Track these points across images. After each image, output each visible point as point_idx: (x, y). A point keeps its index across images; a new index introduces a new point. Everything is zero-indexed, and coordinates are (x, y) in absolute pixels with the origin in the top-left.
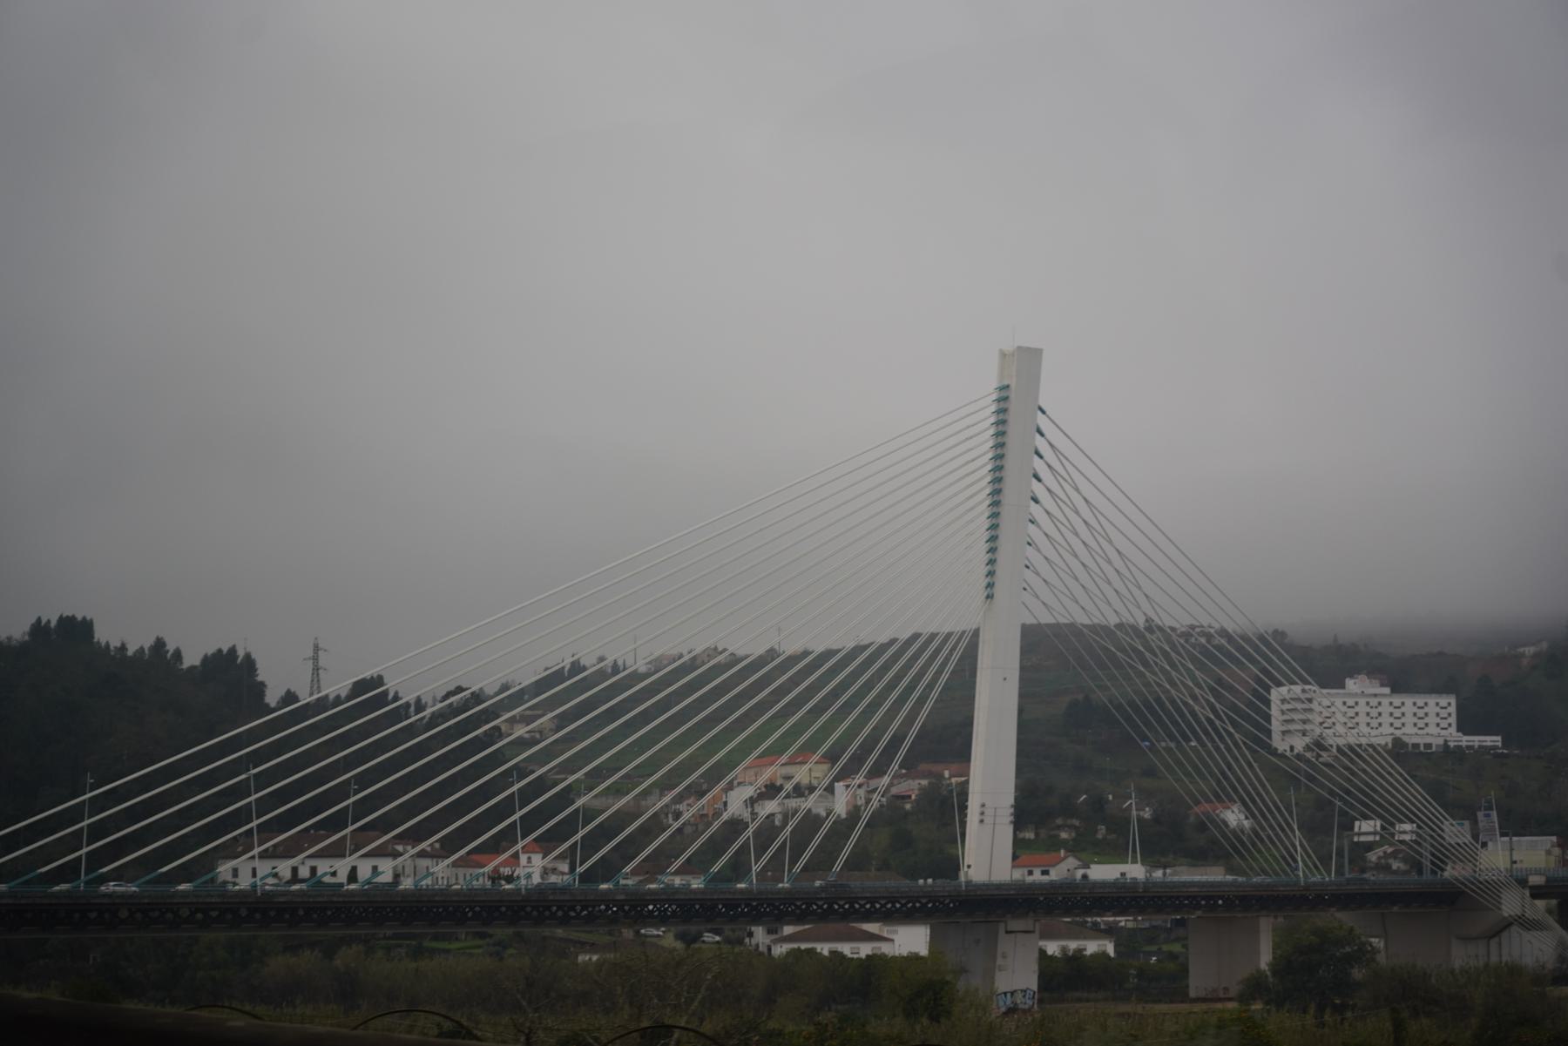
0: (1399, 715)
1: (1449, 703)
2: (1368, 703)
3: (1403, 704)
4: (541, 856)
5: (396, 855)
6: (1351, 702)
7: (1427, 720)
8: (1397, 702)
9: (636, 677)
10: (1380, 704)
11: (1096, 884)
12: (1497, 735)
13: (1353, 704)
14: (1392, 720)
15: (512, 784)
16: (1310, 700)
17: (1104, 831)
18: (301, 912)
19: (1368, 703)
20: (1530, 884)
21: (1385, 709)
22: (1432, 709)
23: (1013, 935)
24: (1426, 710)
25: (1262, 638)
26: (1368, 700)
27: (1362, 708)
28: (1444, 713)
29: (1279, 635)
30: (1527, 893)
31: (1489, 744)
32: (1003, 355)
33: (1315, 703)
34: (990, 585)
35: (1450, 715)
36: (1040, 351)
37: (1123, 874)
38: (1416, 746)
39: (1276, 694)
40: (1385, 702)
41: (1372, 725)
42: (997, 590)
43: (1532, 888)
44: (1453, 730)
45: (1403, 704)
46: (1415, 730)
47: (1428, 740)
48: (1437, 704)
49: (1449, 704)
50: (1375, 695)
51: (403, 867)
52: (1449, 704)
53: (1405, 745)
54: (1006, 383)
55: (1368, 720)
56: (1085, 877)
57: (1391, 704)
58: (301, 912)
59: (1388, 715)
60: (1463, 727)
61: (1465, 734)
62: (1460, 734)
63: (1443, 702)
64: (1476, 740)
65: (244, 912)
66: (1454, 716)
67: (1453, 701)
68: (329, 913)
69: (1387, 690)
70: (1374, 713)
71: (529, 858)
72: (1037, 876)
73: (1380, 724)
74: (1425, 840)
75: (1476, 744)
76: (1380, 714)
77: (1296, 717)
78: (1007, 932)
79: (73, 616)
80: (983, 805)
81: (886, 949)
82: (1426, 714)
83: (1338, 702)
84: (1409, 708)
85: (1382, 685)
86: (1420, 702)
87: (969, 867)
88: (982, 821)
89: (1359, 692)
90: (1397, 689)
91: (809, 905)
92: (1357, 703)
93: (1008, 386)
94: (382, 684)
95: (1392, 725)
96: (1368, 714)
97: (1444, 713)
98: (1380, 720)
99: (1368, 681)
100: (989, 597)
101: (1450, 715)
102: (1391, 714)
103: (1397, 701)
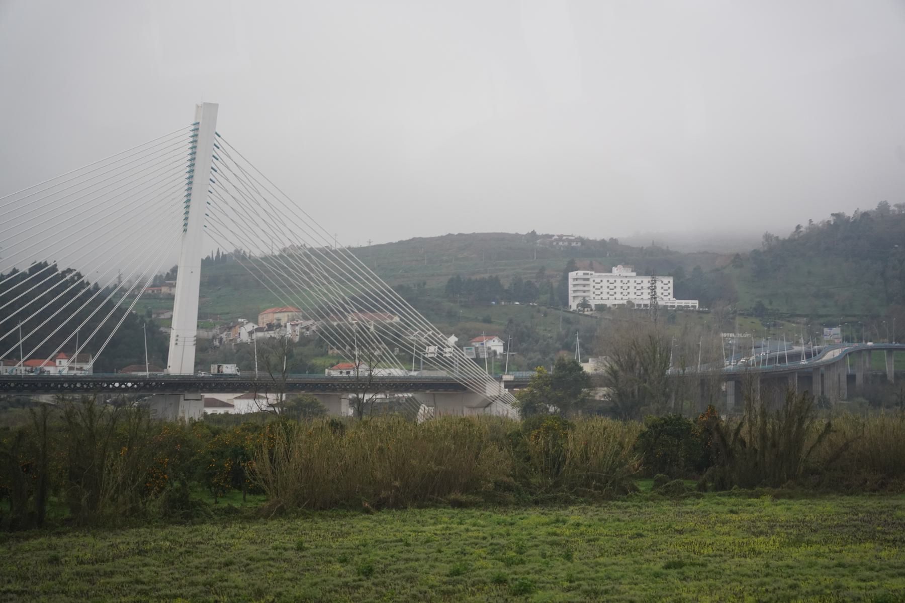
2: (622, 281)
3: (642, 282)
4: (67, 360)
6: (612, 280)
8: (639, 281)
9: (24, 276)
12: (696, 300)
14: (608, 290)
16: (588, 280)
17: (398, 351)
19: (622, 281)
20: (503, 380)
21: (632, 284)
23: (188, 401)
24: (615, 284)
26: (622, 279)
27: (618, 284)
28: (666, 287)
29: (614, 241)
30: (503, 385)
31: (683, 305)
33: (591, 280)
34: (186, 225)
35: (669, 288)
38: (639, 305)
39: (572, 275)
40: (632, 280)
41: (623, 294)
43: (506, 382)
44: (671, 296)
45: (642, 282)
46: (635, 296)
49: (669, 282)
50: (626, 277)
52: (669, 282)
53: (633, 305)
54: (198, 121)
55: (622, 290)
57: (635, 282)
59: (606, 287)
60: (676, 296)
61: (677, 299)
62: (674, 299)
63: (666, 281)
64: (683, 303)
65: (40, 385)
67: (671, 280)
68: (213, 385)
69: (634, 274)
70: (625, 287)
71: (60, 362)
73: (629, 293)
74: (456, 357)
76: (629, 287)
77: (582, 288)
78: (185, 400)
79: (837, 216)
80: (177, 336)
81: (231, 411)
82: (615, 287)
83: (605, 280)
85: (632, 271)
87: (169, 367)
88: (176, 344)
92: (615, 281)
93: (199, 123)
94: (57, 270)
96: (622, 287)
97: (666, 287)
98: (628, 290)
99: (622, 268)
100: (185, 230)
101: (669, 288)
103: (639, 280)
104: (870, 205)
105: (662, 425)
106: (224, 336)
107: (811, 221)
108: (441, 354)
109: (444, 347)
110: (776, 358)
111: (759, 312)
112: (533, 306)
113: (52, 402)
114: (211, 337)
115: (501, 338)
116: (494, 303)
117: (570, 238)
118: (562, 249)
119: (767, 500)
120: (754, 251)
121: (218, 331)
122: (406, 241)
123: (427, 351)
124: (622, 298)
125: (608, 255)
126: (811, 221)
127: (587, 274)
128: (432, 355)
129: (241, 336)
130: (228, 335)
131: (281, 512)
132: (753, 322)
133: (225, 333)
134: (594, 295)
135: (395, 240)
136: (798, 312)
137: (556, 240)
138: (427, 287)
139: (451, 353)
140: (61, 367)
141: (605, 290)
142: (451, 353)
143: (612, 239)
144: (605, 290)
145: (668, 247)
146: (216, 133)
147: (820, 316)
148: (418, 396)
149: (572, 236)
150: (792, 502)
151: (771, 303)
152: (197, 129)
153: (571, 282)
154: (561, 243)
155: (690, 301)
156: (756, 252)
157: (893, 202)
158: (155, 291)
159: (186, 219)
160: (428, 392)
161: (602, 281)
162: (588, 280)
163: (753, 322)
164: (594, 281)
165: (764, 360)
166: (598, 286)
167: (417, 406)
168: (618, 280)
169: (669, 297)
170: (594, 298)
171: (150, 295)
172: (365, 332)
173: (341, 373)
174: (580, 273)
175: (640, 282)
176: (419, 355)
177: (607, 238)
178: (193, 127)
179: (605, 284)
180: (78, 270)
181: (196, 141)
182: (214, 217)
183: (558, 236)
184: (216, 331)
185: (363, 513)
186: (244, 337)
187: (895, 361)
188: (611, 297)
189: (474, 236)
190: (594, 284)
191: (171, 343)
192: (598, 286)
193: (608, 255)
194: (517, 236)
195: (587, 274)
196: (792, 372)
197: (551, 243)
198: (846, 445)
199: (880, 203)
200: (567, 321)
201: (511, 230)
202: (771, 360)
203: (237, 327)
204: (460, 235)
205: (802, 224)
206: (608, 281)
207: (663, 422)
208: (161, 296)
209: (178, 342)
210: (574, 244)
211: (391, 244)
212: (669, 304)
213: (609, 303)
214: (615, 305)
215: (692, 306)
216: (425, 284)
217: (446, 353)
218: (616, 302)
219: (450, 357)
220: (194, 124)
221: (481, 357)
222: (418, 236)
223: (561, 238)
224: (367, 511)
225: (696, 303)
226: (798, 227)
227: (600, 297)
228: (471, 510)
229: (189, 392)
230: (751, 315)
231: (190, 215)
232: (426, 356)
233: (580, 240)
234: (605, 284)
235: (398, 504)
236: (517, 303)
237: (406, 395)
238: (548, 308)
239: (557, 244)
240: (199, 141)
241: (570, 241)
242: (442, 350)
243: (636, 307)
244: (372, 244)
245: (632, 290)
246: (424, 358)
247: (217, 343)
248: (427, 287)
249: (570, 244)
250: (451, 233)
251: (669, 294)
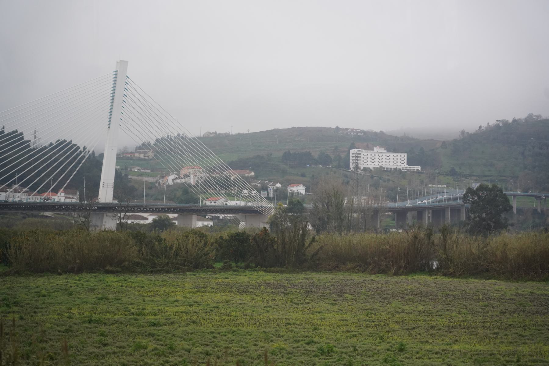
0: (396, 159)
1: (405, 156)
2: (378, 155)
3: (390, 155)
5: (6, 192)
6: (373, 155)
7: (397, 161)
8: (388, 155)
9: (45, 148)
10: (382, 155)
11: (230, 206)
13: (366, 155)
15: (16, 176)
18: (178, 210)
19: (378, 155)
21: (384, 157)
22: (399, 157)
24: (397, 157)
25: (194, 139)
27: (377, 157)
28: (403, 159)
32: (117, 62)
33: (362, 154)
34: (109, 124)
36: (127, 62)
37: (237, 204)
38: (387, 168)
40: (384, 155)
42: (111, 126)
44: (405, 164)
47: (391, 167)
48: (401, 156)
49: (405, 156)
50: (381, 153)
51: (9, 195)
52: (405, 156)
55: (378, 160)
56: (226, 204)
58: (178, 210)
60: (409, 163)
63: (403, 155)
64: (412, 167)
66: (406, 159)
69: (386, 151)
70: (380, 158)
72: (213, 204)
74: (257, 196)
75: (416, 169)
78: (106, 216)
80: (104, 183)
83: (369, 154)
84: (392, 157)
85: (385, 150)
86: (395, 155)
88: (103, 187)
89: (377, 151)
90: (389, 151)
91: (131, 209)
93: (117, 71)
95: (371, 161)
97: (403, 159)
98: (382, 160)
100: (109, 127)
102: (371, 158)
104: (521, 115)
105: (235, 236)
106: (160, 181)
107: (488, 123)
108: (250, 194)
109: (251, 191)
110: (445, 200)
111: (452, 173)
112: (329, 168)
113: (51, 215)
114: (155, 181)
115: (304, 185)
116: (308, 166)
117: (358, 130)
118: (353, 136)
119: (262, 273)
120: (455, 139)
121: (158, 178)
122: (270, 130)
123: (243, 192)
124: (371, 164)
125: (378, 140)
126: (488, 123)
127: (360, 151)
128: (246, 195)
129: (169, 181)
130: (162, 181)
131: (18, 273)
132: (448, 179)
133: (161, 180)
134: (363, 163)
135: (264, 130)
136: (474, 174)
137: (350, 131)
138: (272, 156)
139: (255, 194)
140: (61, 197)
141: (369, 160)
142: (255, 194)
143: (381, 131)
144: (369, 160)
145: (412, 136)
146: (127, 76)
147: (486, 176)
148: (238, 216)
149: (359, 129)
150: (408, 276)
151: (460, 168)
152: (117, 74)
153: (351, 155)
154: (352, 133)
155: (416, 167)
156: (455, 140)
157: (546, 114)
158: (132, 156)
159: (110, 121)
160: (240, 214)
161: (367, 155)
162: (360, 154)
163: (448, 179)
164: (363, 155)
165: (445, 200)
166: (365, 158)
167: (238, 222)
168: (377, 155)
169: (405, 164)
170: (363, 164)
171: (128, 157)
172: (228, 181)
173: (211, 202)
174: (356, 150)
175: (389, 156)
176: (239, 194)
177: (378, 131)
178: (114, 73)
179: (369, 156)
180: (78, 145)
181: (116, 80)
182: (126, 121)
183: (351, 129)
184: (157, 178)
185: (58, 275)
186: (170, 182)
187: (517, 202)
188: (373, 164)
189: (306, 128)
190: (363, 156)
191: (100, 186)
192: (365, 158)
193: (378, 140)
194: (330, 129)
195: (360, 151)
196: (447, 207)
197: (347, 133)
198: (321, 248)
199: (529, 115)
200: (346, 176)
201: (327, 126)
202: (449, 200)
203: (167, 177)
204: (299, 128)
205: (482, 125)
206: (371, 155)
207: (236, 235)
208: (135, 159)
209: (104, 186)
210: (359, 134)
211: (262, 132)
212: (404, 168)
213: (371, 167)
214: (374, 168)
215: (417, 170)
216: (271, 155)
217: (252, 194)
218: (375, 166)
219: (255, 196)
220: (115, 72)
221: (270, 196)
222: (276, 128)
223: (352, 130)
224: (60, 274)
225: (419, 168)
226: (480, 127)
227: (366, 163)
228: (421, 276)
229: (109, 212)
230: (447, 175)
231: (112, 119)
232: (242, 195)
233: (363, 131)
234: (369, 156)
235: (78, 270)
236: (320, 166)
237: (229, 215)
238: (337, 169)
239: (351, 133)
240: (117, 80)
241: (357, 132)
242: (251, 192)
243: (385, 169)
244: (250, 132)
245: (384, 160)
246: (241, 196)
247: (157, 184)
248: (272, 156)
249: (358, 134)
250: (294, 126)
251: (404, 162)
